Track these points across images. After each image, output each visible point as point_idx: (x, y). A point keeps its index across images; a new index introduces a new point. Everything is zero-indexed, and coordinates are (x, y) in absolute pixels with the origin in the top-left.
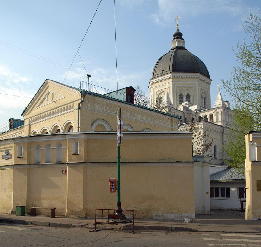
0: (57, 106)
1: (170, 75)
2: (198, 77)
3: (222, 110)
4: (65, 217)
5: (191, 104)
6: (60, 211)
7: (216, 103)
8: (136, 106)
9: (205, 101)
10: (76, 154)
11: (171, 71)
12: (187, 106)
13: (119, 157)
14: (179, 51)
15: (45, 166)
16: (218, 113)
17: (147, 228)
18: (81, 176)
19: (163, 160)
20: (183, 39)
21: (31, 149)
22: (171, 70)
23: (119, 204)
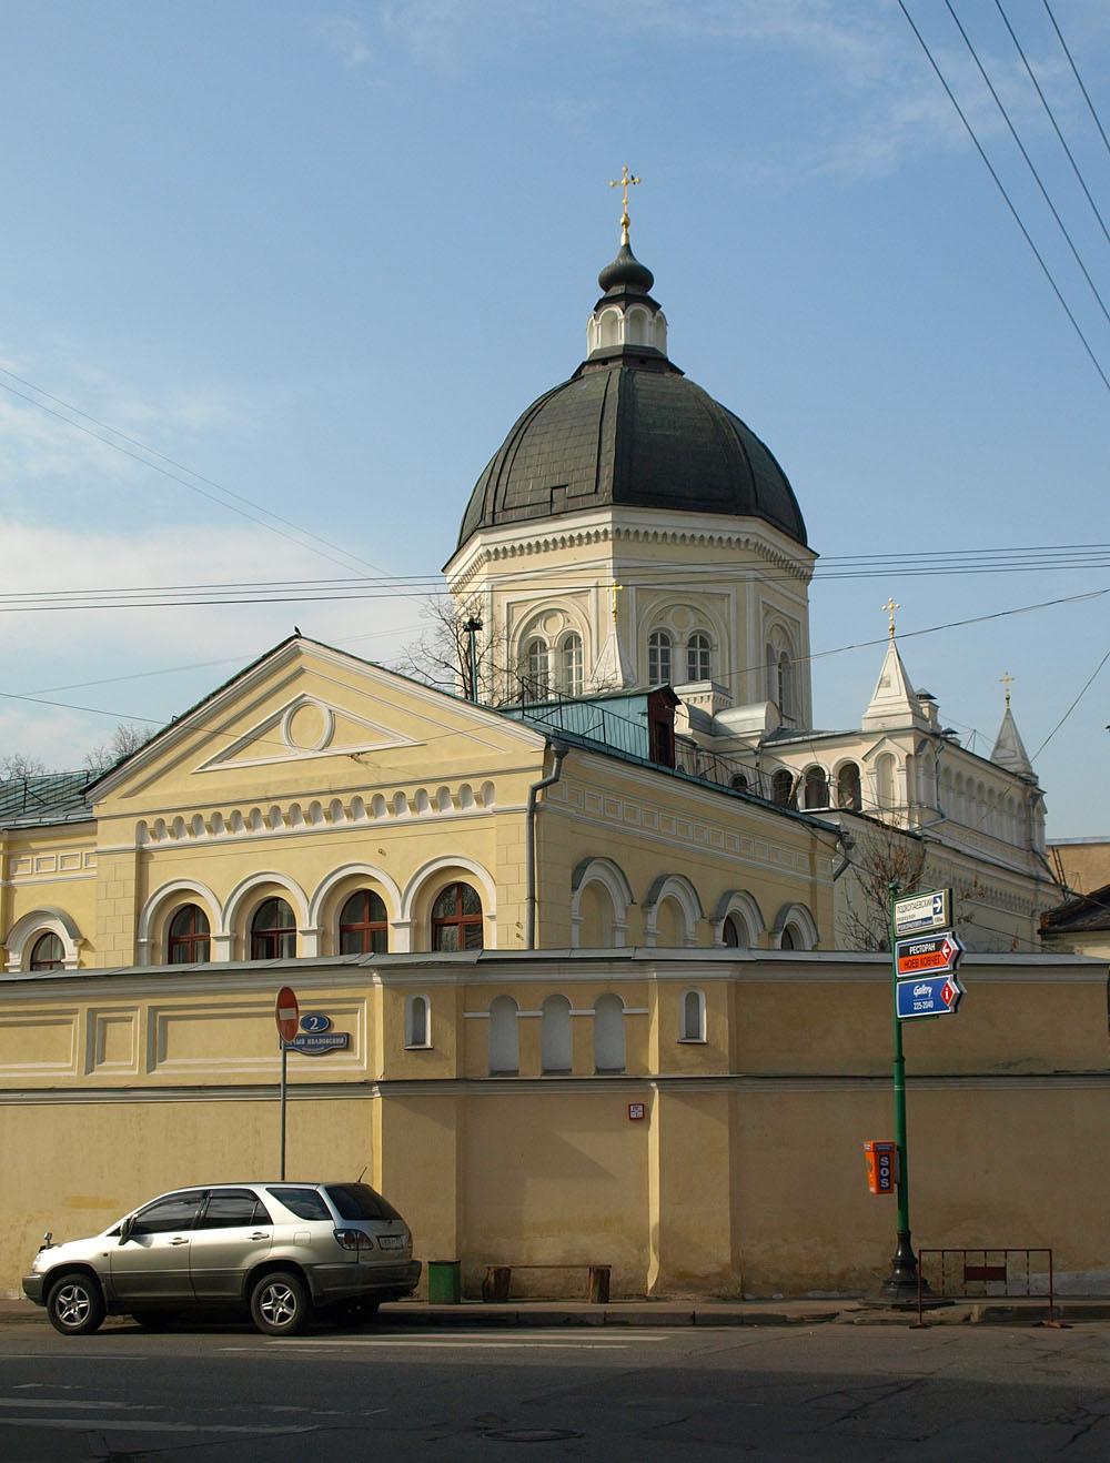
0: (375, 781)
1: (603, 520)
2: (753, 539)
3: (909, 744)
4: (649, 1300)
5: (724, 700)
6: (619, 1279)
7: (873, 703)
8: (480, 707)
9: (780, 673)
10: (691, 1037)
11: (607, 496)
12: (707, 707)
13: (901, 1060)
14: (644, 380)
15: (543, 1090)
16: (887, 758)
17: (1061, 1314)
18: (722, 1133)
19: (1010, 1064)
20: (655, 306)
21: (467, 1015)
22: (610, 488)
23: (905, 1238)
